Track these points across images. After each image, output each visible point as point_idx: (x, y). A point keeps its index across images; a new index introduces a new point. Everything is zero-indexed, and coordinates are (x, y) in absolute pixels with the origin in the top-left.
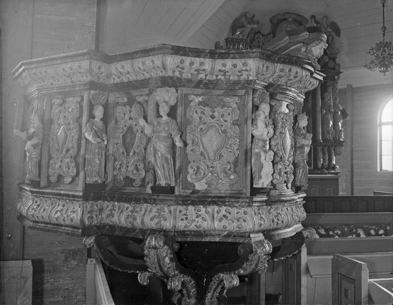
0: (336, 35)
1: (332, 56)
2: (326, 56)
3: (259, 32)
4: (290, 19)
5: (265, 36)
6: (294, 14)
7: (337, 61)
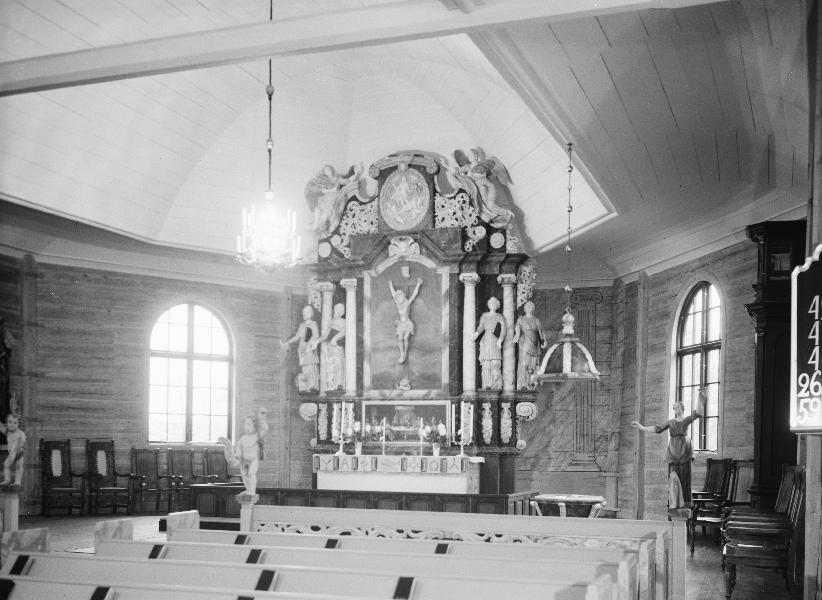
4: (403, 167)
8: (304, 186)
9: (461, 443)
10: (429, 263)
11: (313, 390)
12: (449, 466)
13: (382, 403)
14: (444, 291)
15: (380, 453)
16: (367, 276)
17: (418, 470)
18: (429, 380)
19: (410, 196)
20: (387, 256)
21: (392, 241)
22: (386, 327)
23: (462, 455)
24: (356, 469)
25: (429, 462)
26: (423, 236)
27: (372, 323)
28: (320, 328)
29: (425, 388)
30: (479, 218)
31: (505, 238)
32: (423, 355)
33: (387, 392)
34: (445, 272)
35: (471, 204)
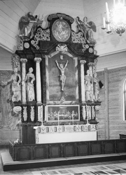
0: (93, 30)
1: (92, 45)
2: (87, 45)
3: (40, 27)
4: (61, 18)
5: (44, 30)
6: (64, 14)
7: (95, 48)
8: (20, 18)
9: (87, 120)
10: (70, 55)
11: (20, 101)
12: (91, 128)
13: (55, 106)
14: (76, 66)
15: (57, 125)
16: (47, 57)
17: (81, 130)
18: (72, 98)
19: (63, 29)
20: (55, 51)
21: (58, 45)
22: (54, 77)
23: (88, 124)
24: (48, 131)
25: (84, 127)
26: (69, 44)
27: (49, 75)
28: (21, 77)
29: (70, 100)
30: (86, 41)
31: (24, 46)
32: (69, 88)
33: (56, 102)
34: (76, 59)
35: (83, 36)
